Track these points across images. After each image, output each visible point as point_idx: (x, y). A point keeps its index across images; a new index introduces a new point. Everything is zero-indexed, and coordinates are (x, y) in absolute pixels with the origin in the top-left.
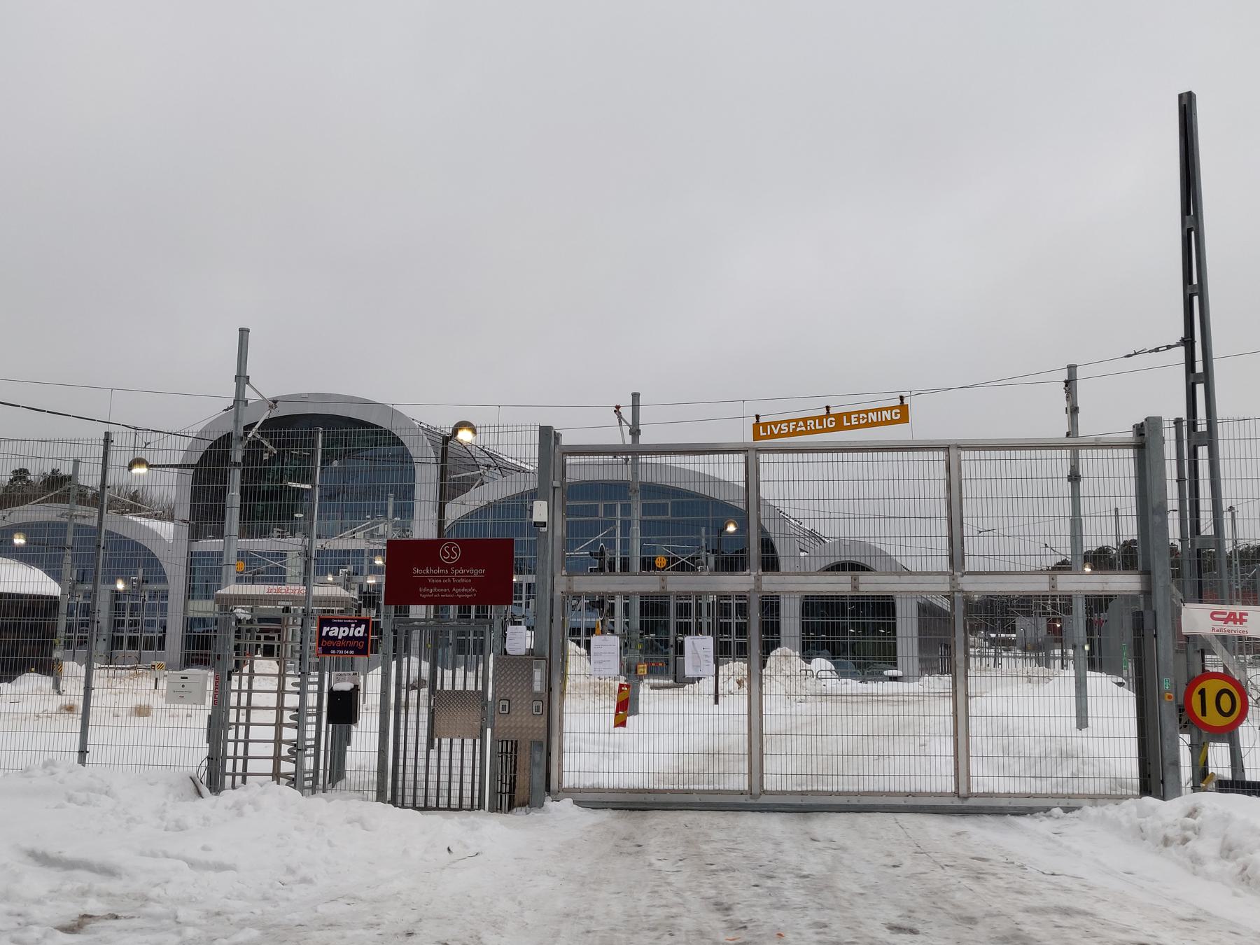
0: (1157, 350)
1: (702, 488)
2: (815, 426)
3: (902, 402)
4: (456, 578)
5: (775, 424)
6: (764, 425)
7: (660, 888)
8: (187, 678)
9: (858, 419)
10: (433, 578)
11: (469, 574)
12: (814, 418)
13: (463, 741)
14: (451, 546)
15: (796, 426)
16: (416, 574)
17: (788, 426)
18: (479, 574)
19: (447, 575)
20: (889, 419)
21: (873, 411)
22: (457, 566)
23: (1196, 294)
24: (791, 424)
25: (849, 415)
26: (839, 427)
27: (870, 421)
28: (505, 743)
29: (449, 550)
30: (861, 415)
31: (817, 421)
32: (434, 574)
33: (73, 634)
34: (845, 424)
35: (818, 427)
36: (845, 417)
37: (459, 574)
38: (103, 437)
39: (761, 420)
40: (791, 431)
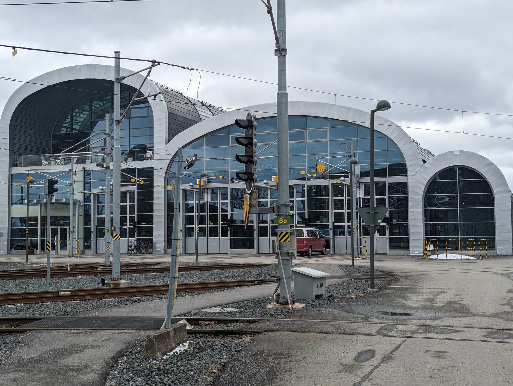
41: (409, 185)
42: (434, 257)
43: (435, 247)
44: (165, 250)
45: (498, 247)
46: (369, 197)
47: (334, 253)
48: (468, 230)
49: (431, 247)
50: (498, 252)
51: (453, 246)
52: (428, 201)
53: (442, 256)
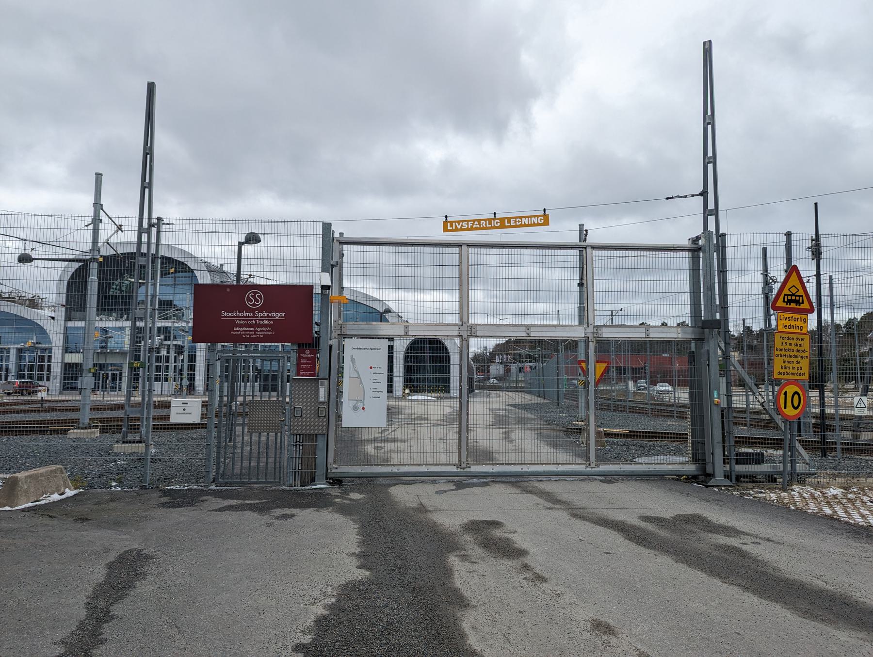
0: (685, 197)
1: (190, 249)
2: (486, 224)
3: (545, 213)
4: (260, 320)
5: (459, 222)
6: (451, 223)
7: (514, 535)
8: (187, 403)
9: (515, 222)
10: (240, 320)
11: (271, 317)
12: (485, 220)
13: (268, 434)
14: (255, 293)
15: (473, 224)
16: (224, 317)
17: (468, 224)
18: (280, 317)
19: (252, 317)
20: (536, 222)
21: (525, 217)
22: (260, 310)
23: (710, 163)
24: (470, 223)
25: (509, 219)
26: (503, 226)
27: (523, 223)
28: (298, 436)
29: (254, 297)
30: (517, 220)
31: (487, 221)
32: (240, 317)
33: (161, 373)
34: (507, 224)
35: (488, 226)
36: (506, 220)
37: (262, 317)
38: (578, 229)
39: (449, 219)
40: (470, 227)
41: (395, 348)
42: (410, 398)
43: (410, 391)
44: (204, 392)
45: (451, 391)
46: (144, 281)
47: (162, 394)
48: (432, 380)
49: (407, 391)
50: (452, 395)
51: (423, 391)
52: (406, 358)
53: (415, 397)
